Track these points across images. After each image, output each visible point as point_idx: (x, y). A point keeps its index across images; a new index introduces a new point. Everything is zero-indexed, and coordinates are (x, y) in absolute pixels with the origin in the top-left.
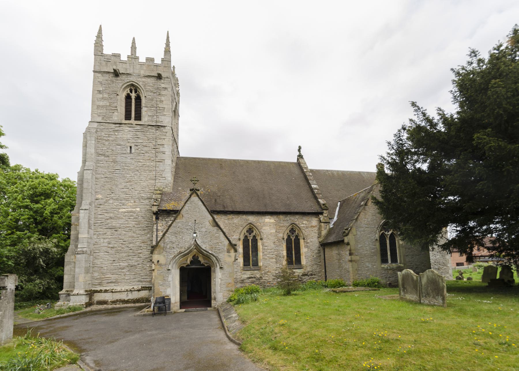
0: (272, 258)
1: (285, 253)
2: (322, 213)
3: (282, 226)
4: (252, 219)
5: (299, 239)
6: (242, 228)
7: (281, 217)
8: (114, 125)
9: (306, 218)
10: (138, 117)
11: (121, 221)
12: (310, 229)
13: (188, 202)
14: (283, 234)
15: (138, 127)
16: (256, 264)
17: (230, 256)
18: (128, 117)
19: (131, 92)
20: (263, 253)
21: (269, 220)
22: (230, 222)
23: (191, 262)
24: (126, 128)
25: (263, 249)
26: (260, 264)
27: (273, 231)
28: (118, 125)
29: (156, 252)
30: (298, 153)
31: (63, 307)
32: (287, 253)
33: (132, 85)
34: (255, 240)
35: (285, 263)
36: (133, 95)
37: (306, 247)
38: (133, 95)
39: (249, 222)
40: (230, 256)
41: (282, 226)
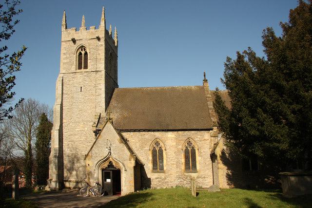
0: (173, 164)
1: (183, 160)
2: (212, 129)
3: (181, 140)
4: (157, 134)
5: (195, 150)
6: (151, 142)
7: (180, 132)
8: (72, 74)
9: (199, 132)
10: (86, 67)
11: (77, 137)
12: (203, 142)
13: (105, 127)
14: (182, 146)
15: (86, 74)
16: (162, 169)
17: (131, 163)
18: (80, 68)
19: (82, 50)
20: (167, 160)
21: (170, 135)
22: (143, 137)
23: (109, 166)
24: (78, 75)
25: (167, 157)
26: (165, 168)
27: (175, 144)
28: (74, 74)
29: (87, 159)
30: (203, 78)
31: (218, 152)
32: (186, 161)
33: (83, 46)
34: (161, 151)
35: (183, 167)
36: (83, 52)
37: (200, 156)
38: (83, 52)
39: (156, 137)
40: (131, 163)
41: (181, 140)
